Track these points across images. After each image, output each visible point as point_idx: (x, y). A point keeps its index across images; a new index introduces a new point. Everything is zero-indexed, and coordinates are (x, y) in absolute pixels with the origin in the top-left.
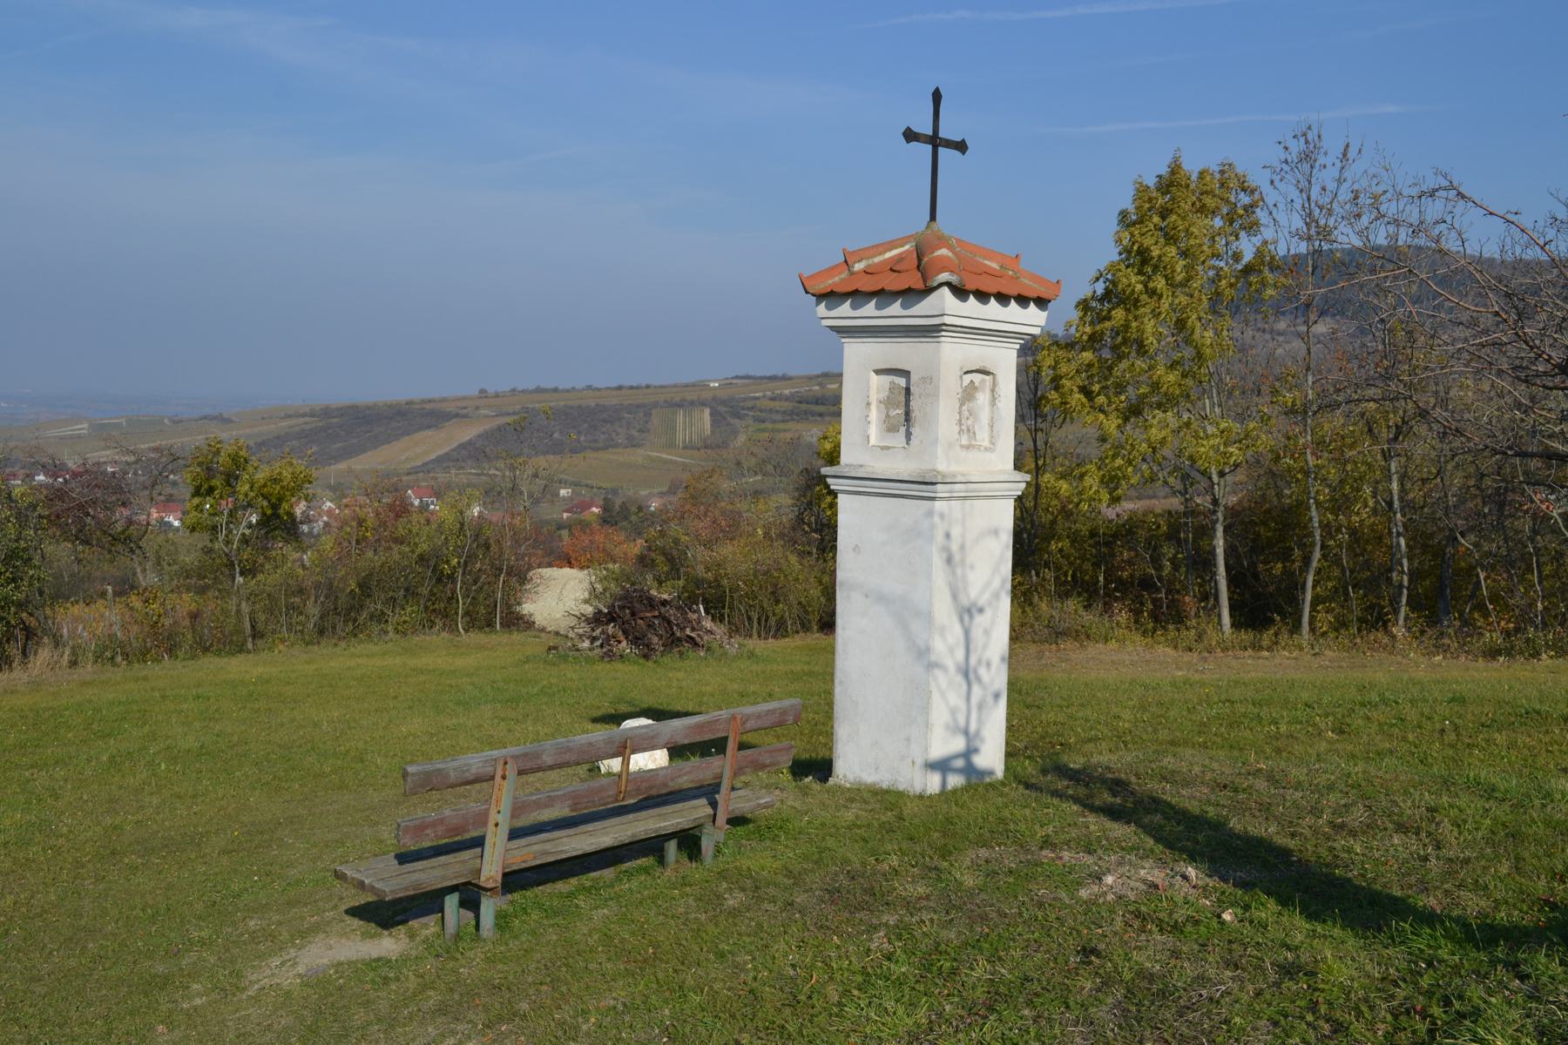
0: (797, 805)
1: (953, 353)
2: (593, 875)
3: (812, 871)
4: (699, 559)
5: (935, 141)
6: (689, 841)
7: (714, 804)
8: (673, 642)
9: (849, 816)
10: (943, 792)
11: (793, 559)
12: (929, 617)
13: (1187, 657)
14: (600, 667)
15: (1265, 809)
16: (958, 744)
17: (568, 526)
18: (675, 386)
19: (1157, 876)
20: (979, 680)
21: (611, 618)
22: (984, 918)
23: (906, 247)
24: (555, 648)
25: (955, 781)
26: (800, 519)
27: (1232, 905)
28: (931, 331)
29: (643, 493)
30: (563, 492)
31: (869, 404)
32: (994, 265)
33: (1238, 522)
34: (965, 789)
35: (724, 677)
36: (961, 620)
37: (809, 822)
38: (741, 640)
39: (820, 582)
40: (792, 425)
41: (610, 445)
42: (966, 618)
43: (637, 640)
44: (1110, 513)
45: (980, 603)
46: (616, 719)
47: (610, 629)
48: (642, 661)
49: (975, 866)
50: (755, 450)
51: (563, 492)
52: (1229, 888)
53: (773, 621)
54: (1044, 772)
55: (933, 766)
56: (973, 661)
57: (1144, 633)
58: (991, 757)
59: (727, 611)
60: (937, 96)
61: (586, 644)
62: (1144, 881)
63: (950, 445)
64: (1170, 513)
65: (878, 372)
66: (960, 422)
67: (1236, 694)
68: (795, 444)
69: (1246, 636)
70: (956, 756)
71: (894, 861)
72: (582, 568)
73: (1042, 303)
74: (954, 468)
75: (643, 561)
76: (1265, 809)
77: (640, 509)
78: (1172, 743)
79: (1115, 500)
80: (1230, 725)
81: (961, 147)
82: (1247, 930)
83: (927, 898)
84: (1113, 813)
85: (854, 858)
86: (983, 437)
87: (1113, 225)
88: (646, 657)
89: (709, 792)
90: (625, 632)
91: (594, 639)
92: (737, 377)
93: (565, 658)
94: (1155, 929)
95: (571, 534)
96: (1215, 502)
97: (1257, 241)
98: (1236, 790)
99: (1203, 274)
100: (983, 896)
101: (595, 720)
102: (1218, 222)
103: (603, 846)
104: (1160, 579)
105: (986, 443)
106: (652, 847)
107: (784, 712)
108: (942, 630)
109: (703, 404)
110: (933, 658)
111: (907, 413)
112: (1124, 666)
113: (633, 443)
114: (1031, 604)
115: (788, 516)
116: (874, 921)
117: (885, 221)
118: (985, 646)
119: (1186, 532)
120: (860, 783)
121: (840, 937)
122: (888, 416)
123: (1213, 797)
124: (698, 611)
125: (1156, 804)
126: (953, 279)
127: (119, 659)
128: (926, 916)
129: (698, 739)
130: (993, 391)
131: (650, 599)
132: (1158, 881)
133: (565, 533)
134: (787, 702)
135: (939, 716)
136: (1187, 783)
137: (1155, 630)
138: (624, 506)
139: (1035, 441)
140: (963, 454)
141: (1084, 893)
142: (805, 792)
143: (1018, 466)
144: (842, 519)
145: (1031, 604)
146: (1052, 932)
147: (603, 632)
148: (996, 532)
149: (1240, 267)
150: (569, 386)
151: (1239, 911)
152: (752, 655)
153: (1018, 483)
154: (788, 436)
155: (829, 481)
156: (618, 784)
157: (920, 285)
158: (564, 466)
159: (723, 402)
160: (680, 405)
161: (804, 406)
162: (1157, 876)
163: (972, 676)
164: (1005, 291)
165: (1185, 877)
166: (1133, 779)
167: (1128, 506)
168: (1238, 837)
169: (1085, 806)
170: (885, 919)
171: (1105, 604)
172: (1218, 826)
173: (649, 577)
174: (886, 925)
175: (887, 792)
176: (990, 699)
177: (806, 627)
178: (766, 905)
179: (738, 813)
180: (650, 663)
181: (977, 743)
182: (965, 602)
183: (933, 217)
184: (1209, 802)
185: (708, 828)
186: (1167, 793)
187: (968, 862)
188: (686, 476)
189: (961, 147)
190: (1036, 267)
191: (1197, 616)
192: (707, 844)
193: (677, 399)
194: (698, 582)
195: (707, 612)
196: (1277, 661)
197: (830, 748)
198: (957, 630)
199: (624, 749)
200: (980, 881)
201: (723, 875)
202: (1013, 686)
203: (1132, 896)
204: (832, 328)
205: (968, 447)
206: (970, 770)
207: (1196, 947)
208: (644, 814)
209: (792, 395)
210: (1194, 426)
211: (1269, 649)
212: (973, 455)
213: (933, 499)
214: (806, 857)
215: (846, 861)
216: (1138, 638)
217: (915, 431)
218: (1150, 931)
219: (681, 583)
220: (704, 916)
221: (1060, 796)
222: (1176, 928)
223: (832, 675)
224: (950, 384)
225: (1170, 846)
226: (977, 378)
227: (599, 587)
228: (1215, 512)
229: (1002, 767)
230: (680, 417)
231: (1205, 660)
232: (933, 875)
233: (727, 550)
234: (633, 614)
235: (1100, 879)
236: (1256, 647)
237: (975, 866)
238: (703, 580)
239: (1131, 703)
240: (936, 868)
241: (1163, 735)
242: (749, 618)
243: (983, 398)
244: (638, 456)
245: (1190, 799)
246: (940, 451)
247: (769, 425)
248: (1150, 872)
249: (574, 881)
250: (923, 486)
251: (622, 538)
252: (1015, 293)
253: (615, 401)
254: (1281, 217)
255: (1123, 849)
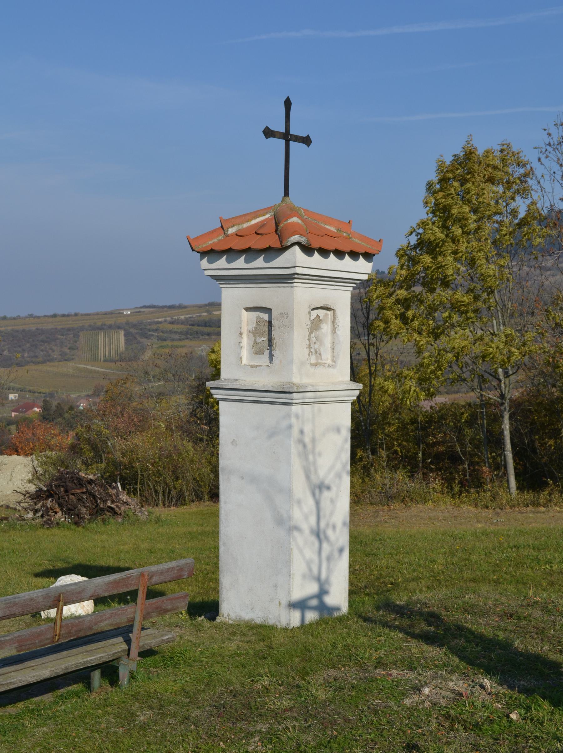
0: (193, 639)
1: (303, 295)
2: (35, 699)
3: (204, 691)
4: (117, 446)
5: (287, 137)
6: (110, 671)
7: (128, 641)
8: (97, 512)
9: (232, 646)
10: (303, 625)
11: (190, 446)
12: (288, 492)
13: (485, 513)
14: (40, 532)
15: (541, 632)
16: (313, 588)
17: (16, 422)
18: (97, 314)
19: (462, 686)
20: (327, 538)
21: (49, 494)
22: (333, 724)
23: (267, 216)
24: (6, 519)
25: (311, 616)
26: (193, 414)
27: (517, 707)
28: (287, 279)
29: (74, 396)
30: (12, 396)
31: (241, 334)
32: (333, 229)
33: (519, 410)
34: (318, 623)
35: (135, 537)
36: (314, 494)
37: (201, 653)
38: (150, 509)
39: (210, 463)
40: (186, 343)
41: (48, 359)
42: (317, 491)
43: (69, 511)
44: (426, 405)
45: (327, 482)
46: (56, 573)
47: (49, 503)
48: (73, 527)
49: (327, 684)
50: (158, 362)
51: (12, 396)
52: (516, 694)
53: (174, 493)
54: (378, 608)
55: (293, 605)
56: (323, 524)
57: (453, 497)
58: (339, 597)
59: (139, 486)
60: (288, 104)
61: (30, 515)
62: (452, 691)
63: (302, 364)
64: (469, 405)
65: (247, 309)
66: (309, 346)
67: (521, 541)
68: (189, 357)
69: (528, 496)
70: (312, 597)
71: (266, 681)
72: (27, 455)
73: (368, 256)
74: (305, 381)
75: (74, 449)
76: (541, 632)
77: (71, 408)
78: (474, 580)
79: (430, 395)
80: (517, 565)
81: (307, 141)
82: (529, 726)
83: (291, 709)
84: (428, 639)
85: (234, 680)
86: (327, 357)
87: (422, 192)
88: (77, 524)
89: (124, 632)
90: (60, 505)
91: (36, 511)
92: (145, 307)
93: (13, 527)
94: (461, 728)
95: (18, 428)
96: (502, 396)
97: (528, 202)
98: (519, 618)
99: (488, 227)
100: (333, 706)
101: (37, 575)
102: (501, 189)
103: (43, 677)
104: (464, 454)
105: (329, 362)
106: (82, 676)
107: (181, 569)
108: (299, 502)
109: (119, 327)
110: (292, 523)
111: (270, 340)
112: (438, 520)
113: (65, 358)
114: (368, 475)
115: (184, 414)
116: (251, 729)
117: (251, 198)
118: (332, 514)
119: (483, 417)
120: (240, 620)
121: (225, 742)
122: (255, 342)
123: (502, 624)
124: (117, 487)
125: (460, 630)
126: (302, 240)
128: (290, 724)
129: (115, 592)
130: (333, 322)
131: (80, 479)
132: (463, 691)
133: (13, 428)
134: (183, 562)
135: (299, 567)
136: (483, 614)
137: (461, 492)
138: (59, 406)
139: (368, 354)
140: (312, 370)
141: (407, 702)
142: (198, 628)
143: (354, 377)
144: (223, 420)
145: (368, 475)
146: (384, 733)
147: (43, 506)
148: (338, 430)
149: (516, 221)
150: (15, 315)
151: (523, 711)
152: (158, 521)
153: (354, 391)
154: (183, 351)
155: (213, 391)
156: (54, 629)
157: (277, 245)
158: (12, 376)
159: (134, 326)
160: (101, 328)
161: (195, 328)
162: (462, 686)
163: (322, 536)
164: (341, 248)
165: (482, 687)
166: (443, 612)
167: (440, 399)
168: (521, 654)
169: (408, 634)
170: (258, 727)
171: (424, 474)
172: (506, 646)
173: (79, 462)
174: (260, 732)
175: (261, 626)
176: (336, 554)
177: (199, 498)
178: (168, 720)
179: (147, 647)
180: (80, 529)
181: (326, 587)
183: (287, 193)
184: (499, 628)
185: (124, 661)
186: (470, 623)
187: (321, 681)
188: (106, 383)
189: (307, 141)
190: (363, 230)
191: (492, 481)
192: (124, 673)
193: (99, 324)
194: (116, 465)
195: (123, 488)
196: (551, 514)
197: (217, 591)
198: (310, 502)
199: (59, 600)
200: (330, 694)
201: (135, 697)
202: (354, 539)
203: (443, 703)
204: (212, 277)
205: (316, 365)
206: (322, 607)
207: (491, 741)
208: (74, 651)
209: (187, 319)
210: (487, 339)
211: (545, 505)
212: (319, 370)
213: (290, 404)
214: (199, 681)
215: (229, 683)
216: (448, 499)
217: (276, 353)
218: (457, 730)
219: (103, 465)
220: (121, 730)
221: (390, 627)
222: (477, 726)
223: (218, 533)
224: (301, 319)
225: (471, 663)
226: (321, 313)
227: (40, 470)
228: (502, 404)
229: (347, 604)
230: (101, 338)
231: (498, 514)
232: (294, 691)
233: (137, 440)
234: (66, 491)
235: (419, 690)
236: (536, 504)
237: (327, 684)
238: (121, 463)
239: (443, 550)
240: (297, 686)
241: (467, 574)
242: (156, 492)
243: (326, 328)
244: (69, 367)
245: (484, 626)
246: (295, 369)
247: (169, 343)
248: (457, 684)
249: (20, 705)
250: (283, 395)
251: (57, 431)
252: (349, 250)
253: (50, 326)
254: (547, 185)
255: (436, 666)
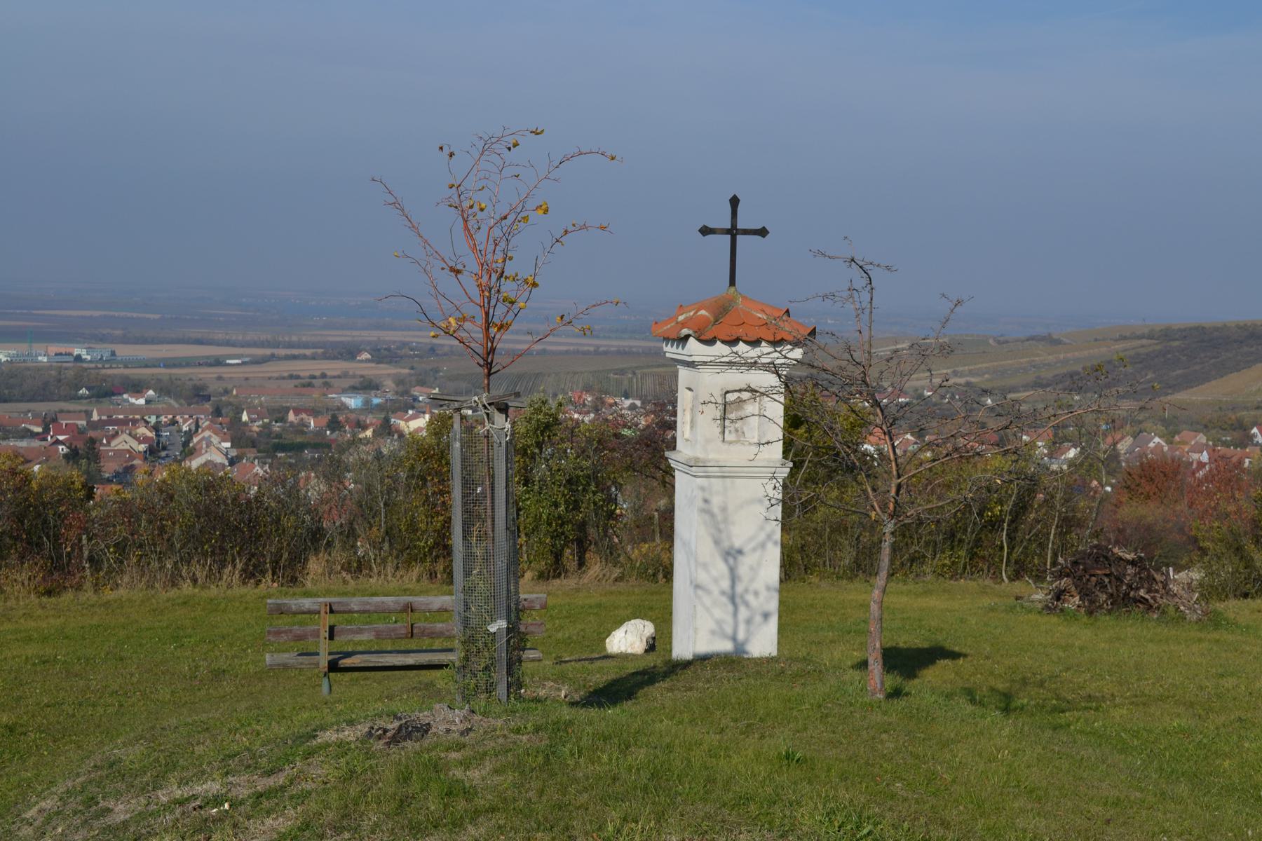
36: (726, 561)
43: (1085, 594)
118: (752, 580)
127: (660, 576)
163: (738, 600)
176: (758, 619)
182: (726, 544)
183: (732, 282)
